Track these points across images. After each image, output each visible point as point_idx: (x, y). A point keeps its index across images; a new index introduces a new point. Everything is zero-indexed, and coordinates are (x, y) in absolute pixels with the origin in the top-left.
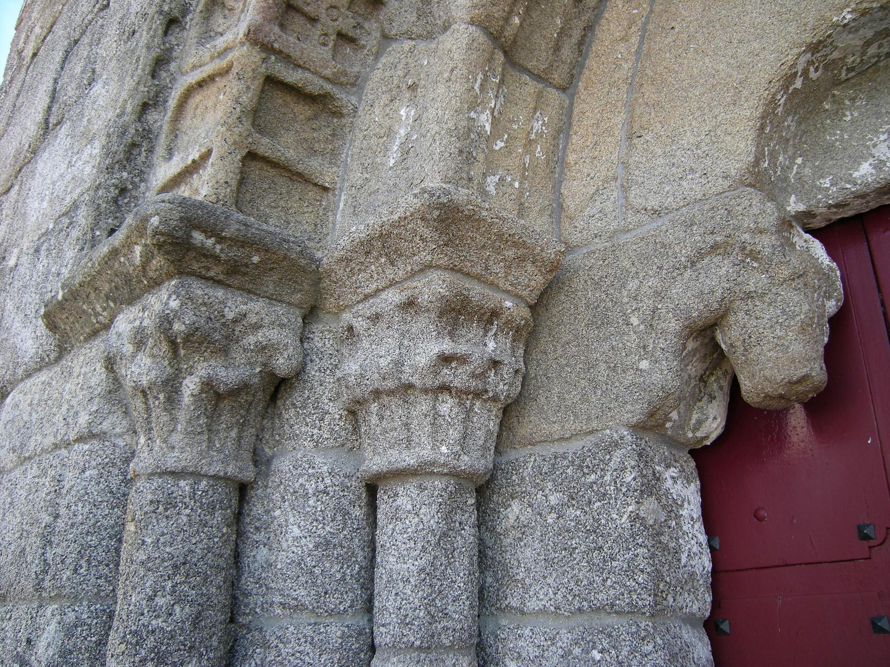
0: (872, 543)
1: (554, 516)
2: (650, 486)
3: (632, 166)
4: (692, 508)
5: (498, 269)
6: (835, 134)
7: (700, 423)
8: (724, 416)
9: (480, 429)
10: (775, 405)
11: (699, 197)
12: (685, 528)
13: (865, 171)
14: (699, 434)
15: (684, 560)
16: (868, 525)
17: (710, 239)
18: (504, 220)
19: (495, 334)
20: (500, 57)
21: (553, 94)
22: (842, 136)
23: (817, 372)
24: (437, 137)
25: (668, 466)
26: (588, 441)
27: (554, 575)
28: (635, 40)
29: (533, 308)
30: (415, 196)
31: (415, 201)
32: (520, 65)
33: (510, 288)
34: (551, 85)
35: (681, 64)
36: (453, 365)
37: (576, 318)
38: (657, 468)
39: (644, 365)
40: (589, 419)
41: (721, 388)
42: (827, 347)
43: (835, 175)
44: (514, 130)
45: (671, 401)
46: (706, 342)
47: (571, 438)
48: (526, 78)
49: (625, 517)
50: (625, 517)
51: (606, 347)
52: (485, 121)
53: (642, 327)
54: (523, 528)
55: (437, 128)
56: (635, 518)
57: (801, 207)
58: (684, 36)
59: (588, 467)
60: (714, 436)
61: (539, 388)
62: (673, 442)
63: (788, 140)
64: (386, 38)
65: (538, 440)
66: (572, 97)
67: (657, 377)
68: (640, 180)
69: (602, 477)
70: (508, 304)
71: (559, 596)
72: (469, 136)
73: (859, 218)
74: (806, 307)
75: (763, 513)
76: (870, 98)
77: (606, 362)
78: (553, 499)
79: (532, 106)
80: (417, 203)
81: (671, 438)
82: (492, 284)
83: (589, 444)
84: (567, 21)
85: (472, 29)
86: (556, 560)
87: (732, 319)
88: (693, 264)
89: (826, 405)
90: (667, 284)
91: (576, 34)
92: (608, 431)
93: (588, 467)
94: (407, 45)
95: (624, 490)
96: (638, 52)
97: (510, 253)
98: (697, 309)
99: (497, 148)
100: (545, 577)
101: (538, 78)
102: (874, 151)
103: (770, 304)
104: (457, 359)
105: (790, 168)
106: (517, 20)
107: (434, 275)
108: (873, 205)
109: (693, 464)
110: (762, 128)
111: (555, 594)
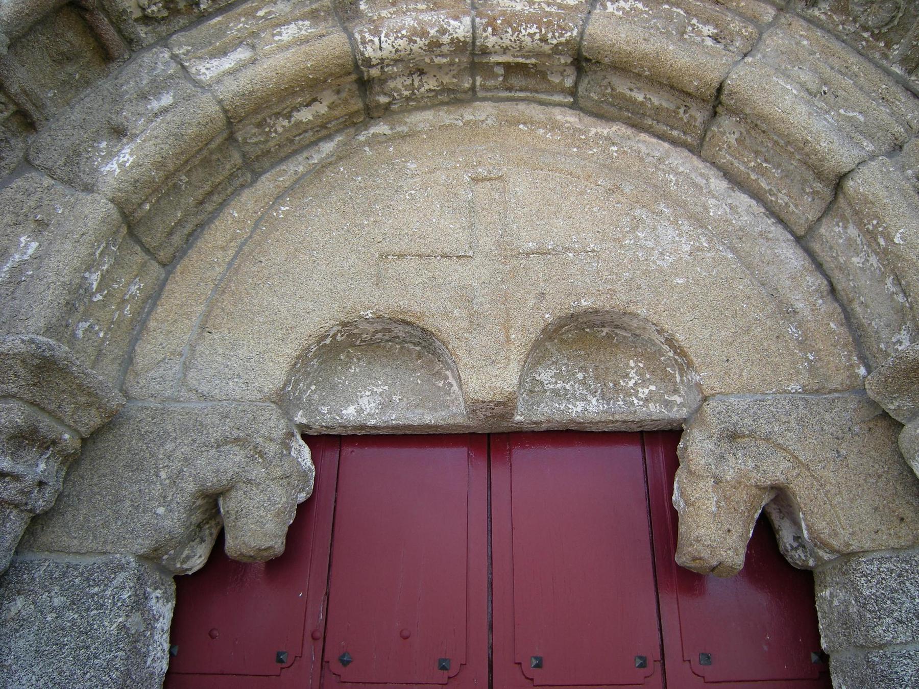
0: (284, 665)
1: (54, 615)
2: (139, 603)
3: (198, 353)
4: (165, 623)
5: (69, 409)
6: (341, 379)
7: (188, 558)
8: (207, 555)
9: (10, 533)
10: (245, 560)
11: (237, 398)
12: (156, 638)
13: (350, 411)
14: (185, 566)
15: (148, 663)
16: (284, 653)
17: (236, 433)
18: (87, 375)
19: (48, 458)
20: (124, 230)
21: (154, 267)
22: (345, 381)
23: (278, 545)
24: (52, 286)
25: (156, 589)
26: (100, 560)
27: (41, 665)
28: (231, 252)
29: (84, 440)
30: (23, 341)
31: (22, 346)
32: (136, 237)
33: (72, 424)
34: (155, 259)
35: (257, 293)
36: (7, 480)
37: (117, 457)
38: (148, 589)
39: (161, 510)
40: (105, 542)
41: (211, 534)
42: (290, 527)
43: (332, 407)
44: (114, 289)
45: (173, 543)
46: (211, 506)
47: (85, 554)
48: (138, 248)
49: (115, 625)
50: (115, 625)
51: (135, 488)
52: (94, 279)
53: (167, 481)
54: (21, 621)
55: (54, 278)
56: (122, 628)
57: (304, 421)
58: (266, 272)
59: (94, 580)
60: (195, 569)
61: (69, 506)
62: (163, 570)
63: (310, 373)
64: (27, 163)
65: (56, 548)
66: (169, 273)
67: (168, 523)
68: (200, 367)
69: (104, 591)
70: (67, 436)
71: (41, 683)
72: (78, 291)
73: (339, 437)
74: (284, 500)
75: (216, 633)
76: (369, 363)
77: (132, 500)
78: (57, 601)
79: (134, 273)
80: (23, 348)
81: (164, 566)
82: (59, 419)
83: (100, 562)
84: (186, 215)
85: (111, 205)
86: (46, 653)
87: (233, 493)
88: (219, 446)
89: (278, 567)
90: (196, 455)
91: (189, 227)
92: (118, 556)
93: (94, 580)
94: (47, 181)
95: (119, 604)
96: (230, 264)
97: (83, 399)
98: (212, 481)
99: (95, 300)
100: (31, 666)
101: (147, 251)
102: (360, 400)
103: (262, 491)
104: (12, 476)
105: (306, 391)
106: (148, 207)
107: (14, 405)
108: (349, 433)
109: (174, 587)
110: (295, 364)
111: (37, 681)
